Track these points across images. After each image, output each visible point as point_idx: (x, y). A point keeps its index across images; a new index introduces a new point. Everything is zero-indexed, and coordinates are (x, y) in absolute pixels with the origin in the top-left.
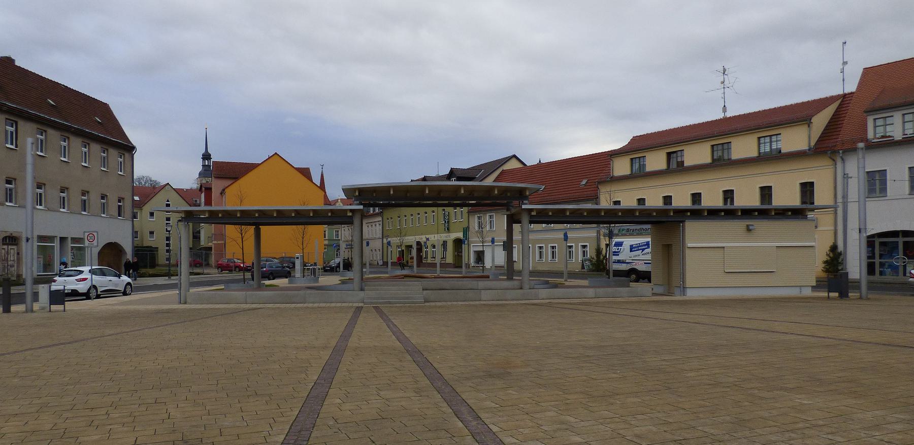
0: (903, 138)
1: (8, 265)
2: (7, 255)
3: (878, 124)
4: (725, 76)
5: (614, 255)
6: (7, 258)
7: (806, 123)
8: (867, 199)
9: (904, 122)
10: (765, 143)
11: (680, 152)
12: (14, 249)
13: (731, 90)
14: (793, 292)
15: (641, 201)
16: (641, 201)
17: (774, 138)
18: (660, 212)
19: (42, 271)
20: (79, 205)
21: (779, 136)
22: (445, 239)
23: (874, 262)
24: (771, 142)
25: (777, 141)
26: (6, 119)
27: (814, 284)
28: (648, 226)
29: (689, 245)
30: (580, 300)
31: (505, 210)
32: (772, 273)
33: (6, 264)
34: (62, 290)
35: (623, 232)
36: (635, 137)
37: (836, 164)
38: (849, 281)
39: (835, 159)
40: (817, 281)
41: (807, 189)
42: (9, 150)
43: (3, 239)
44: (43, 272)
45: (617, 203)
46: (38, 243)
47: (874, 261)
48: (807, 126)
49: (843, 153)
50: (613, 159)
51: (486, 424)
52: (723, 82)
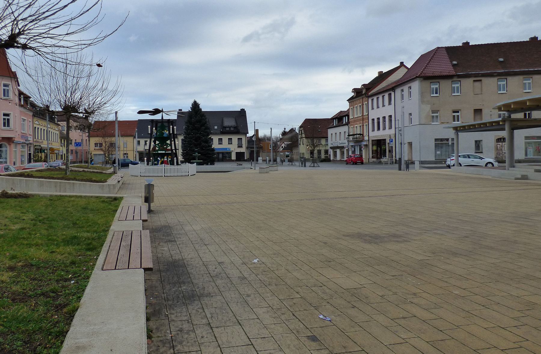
1: (502, 153)
2: (501, 148)
5: (8, 126)
6: (502, 149)
12: (500, 144)
19: (532, 155)
20: (452, 118)
23: (434, 94)
26: (474, 81)
30: (472, 175)
31: (31, 114)
32: (396, 134)
33: (501, 152)
34: (314, 157)
42: (500, 94)
43: (497, 139)
44: (533, 156)
46: (525, 140)
47: (527, 89)
51: (233, 250)
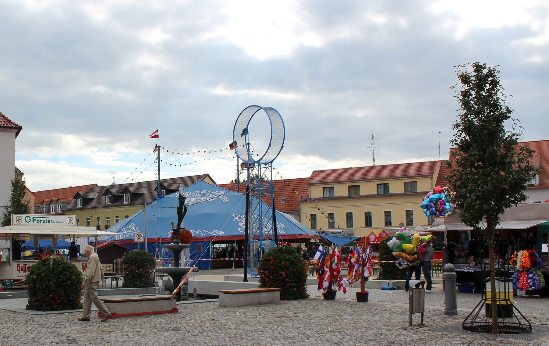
48: (431, 179)
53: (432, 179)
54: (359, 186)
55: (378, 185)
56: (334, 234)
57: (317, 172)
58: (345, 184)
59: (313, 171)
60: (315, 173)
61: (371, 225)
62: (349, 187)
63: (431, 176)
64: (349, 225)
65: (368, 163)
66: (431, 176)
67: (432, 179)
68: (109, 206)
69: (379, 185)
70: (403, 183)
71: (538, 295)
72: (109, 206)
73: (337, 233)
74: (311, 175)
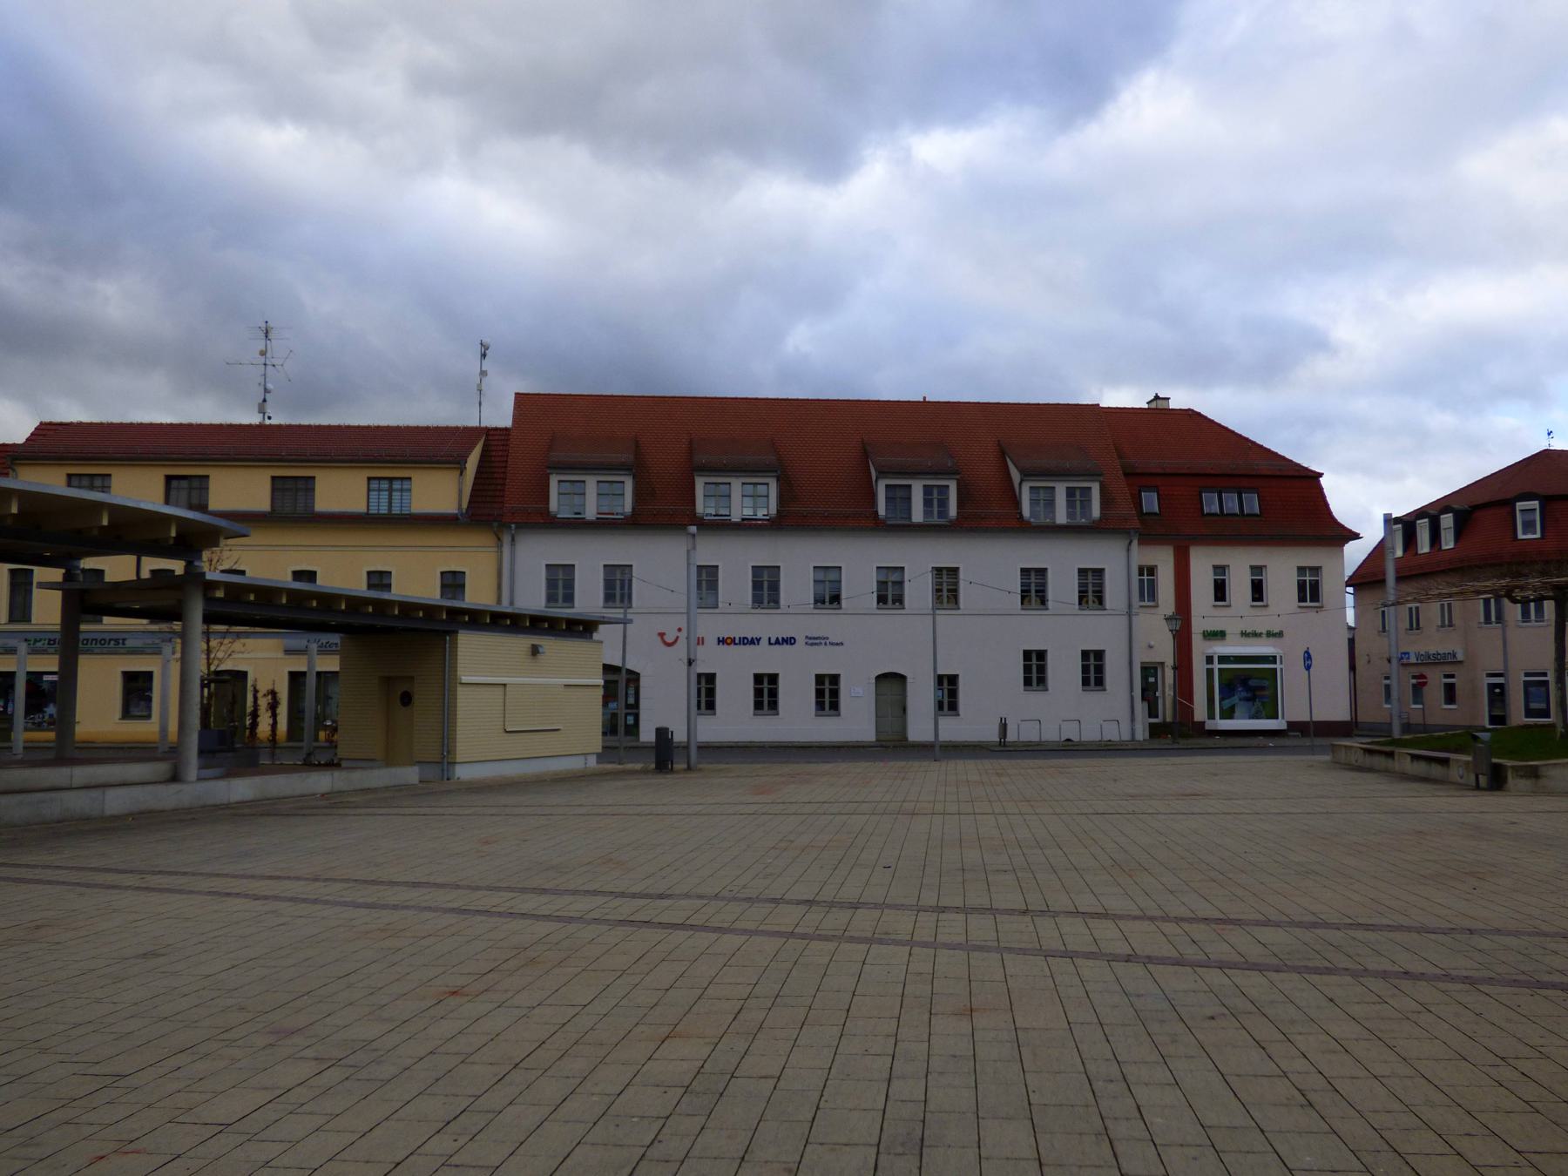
0: (598, 518)
3: (372, 486)
4: (268, 342)
7: (458, 468)
8: (938, 612)
9: (369, 490)
10: (379, 490)
11: (100, 478)
13: (278, 372)
14: (575, 764)
15: (379, 579)
16: (379, 579)
17: (396, 485)
18: (355, 603)
21: (405, 482)
22: (1201, 636)
24: (391, 490)
25: (402, 490)
27: (600, 750)
28: (335, 638)
29: (465, 679)
35: (39, 644)
36: (46, 424)
37: (502, 546)
38: (675, 745)
39: (500, 536)
40: (603, 747)
41: (618, 584)
45: (310, 576)
48: (458, 472)
49: (516, 528)
50: (15, 468)
52: (263, 353)
53: (461, 474)
54: (314, 478)
55: (369, 479)
56: (99, 645)
57: (54, 427)
58: (261, 470)
59: (41, 423)
60: (46, 430)
61: (775, 601)
62: (169, 479)
63: (458, 463)
64: (1219, 595)
65: (253, 419)
66: (458, 463)
67: (461, 474)
68: (184, 628)
69: (174, 483)
70: (366, 479)
71: (1298, 734)
72: (184, 628)
73: (110, 640)
74: (33, 430)
